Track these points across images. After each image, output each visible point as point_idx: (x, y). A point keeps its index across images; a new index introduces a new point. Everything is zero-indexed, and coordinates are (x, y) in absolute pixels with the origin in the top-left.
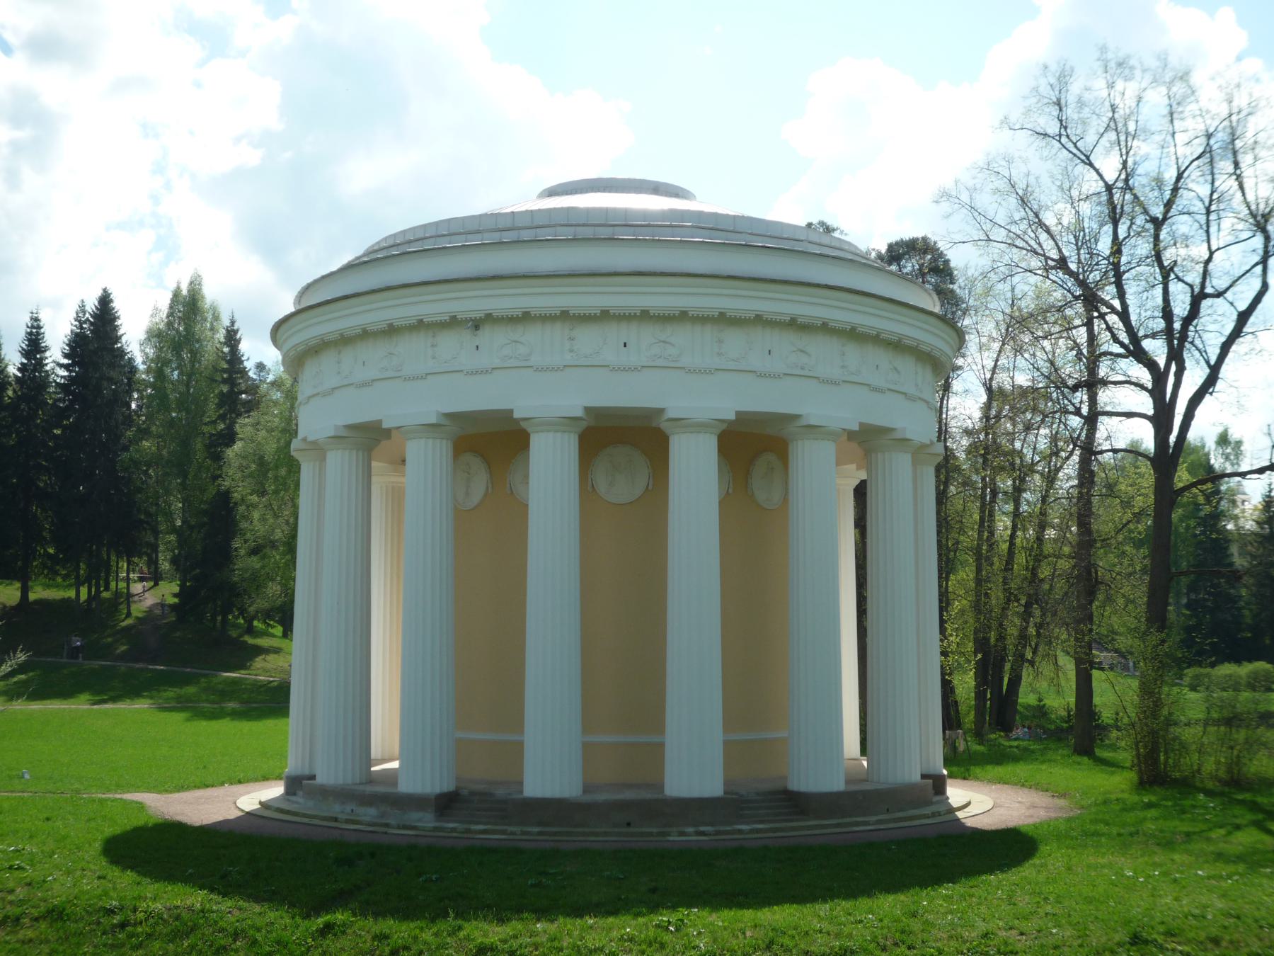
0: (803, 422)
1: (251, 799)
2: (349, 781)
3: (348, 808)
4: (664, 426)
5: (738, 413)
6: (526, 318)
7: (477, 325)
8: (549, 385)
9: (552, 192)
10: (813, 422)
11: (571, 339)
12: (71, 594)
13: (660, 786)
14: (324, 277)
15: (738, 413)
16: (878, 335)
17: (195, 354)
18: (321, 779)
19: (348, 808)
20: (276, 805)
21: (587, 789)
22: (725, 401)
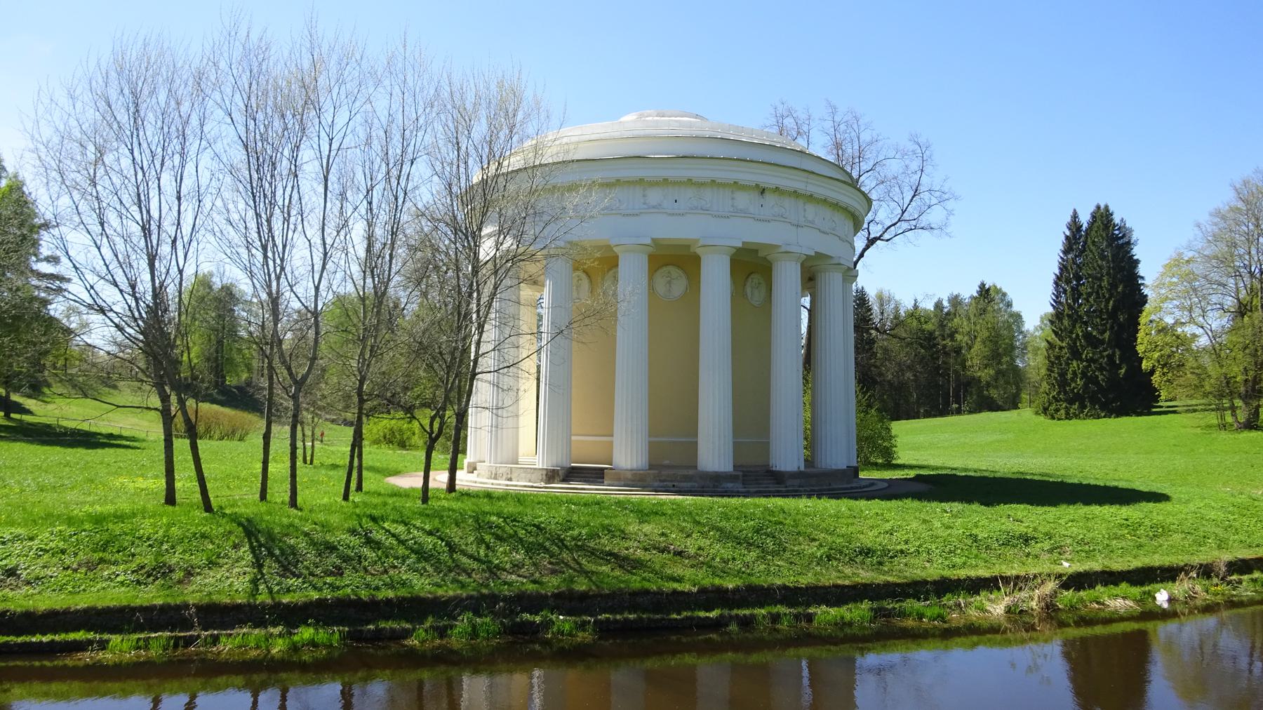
4: (699, 251)
5: (653, 240)
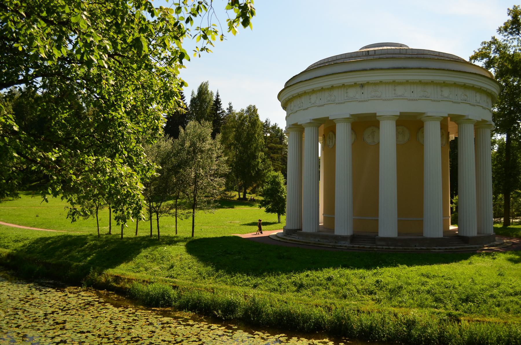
0: (426, 115)
1: (275, 233)
2: (314, 231)
3: (317, 240)
5: (400, 113)
6: (332, 88)
7: (362, 86)
8: (387, 104)
9: (361, 49)
10: (429, 115)
11: (395, 90)
12: (514, 221)
13: (422, 234)
14: (301, 73)
15: (400, 113)
16: (480, 89)
17: (156, 102)
18: (304, 230)
19: (317, 240)
20: (279, 236)
21: (399, 234)
22: (444, 109)
